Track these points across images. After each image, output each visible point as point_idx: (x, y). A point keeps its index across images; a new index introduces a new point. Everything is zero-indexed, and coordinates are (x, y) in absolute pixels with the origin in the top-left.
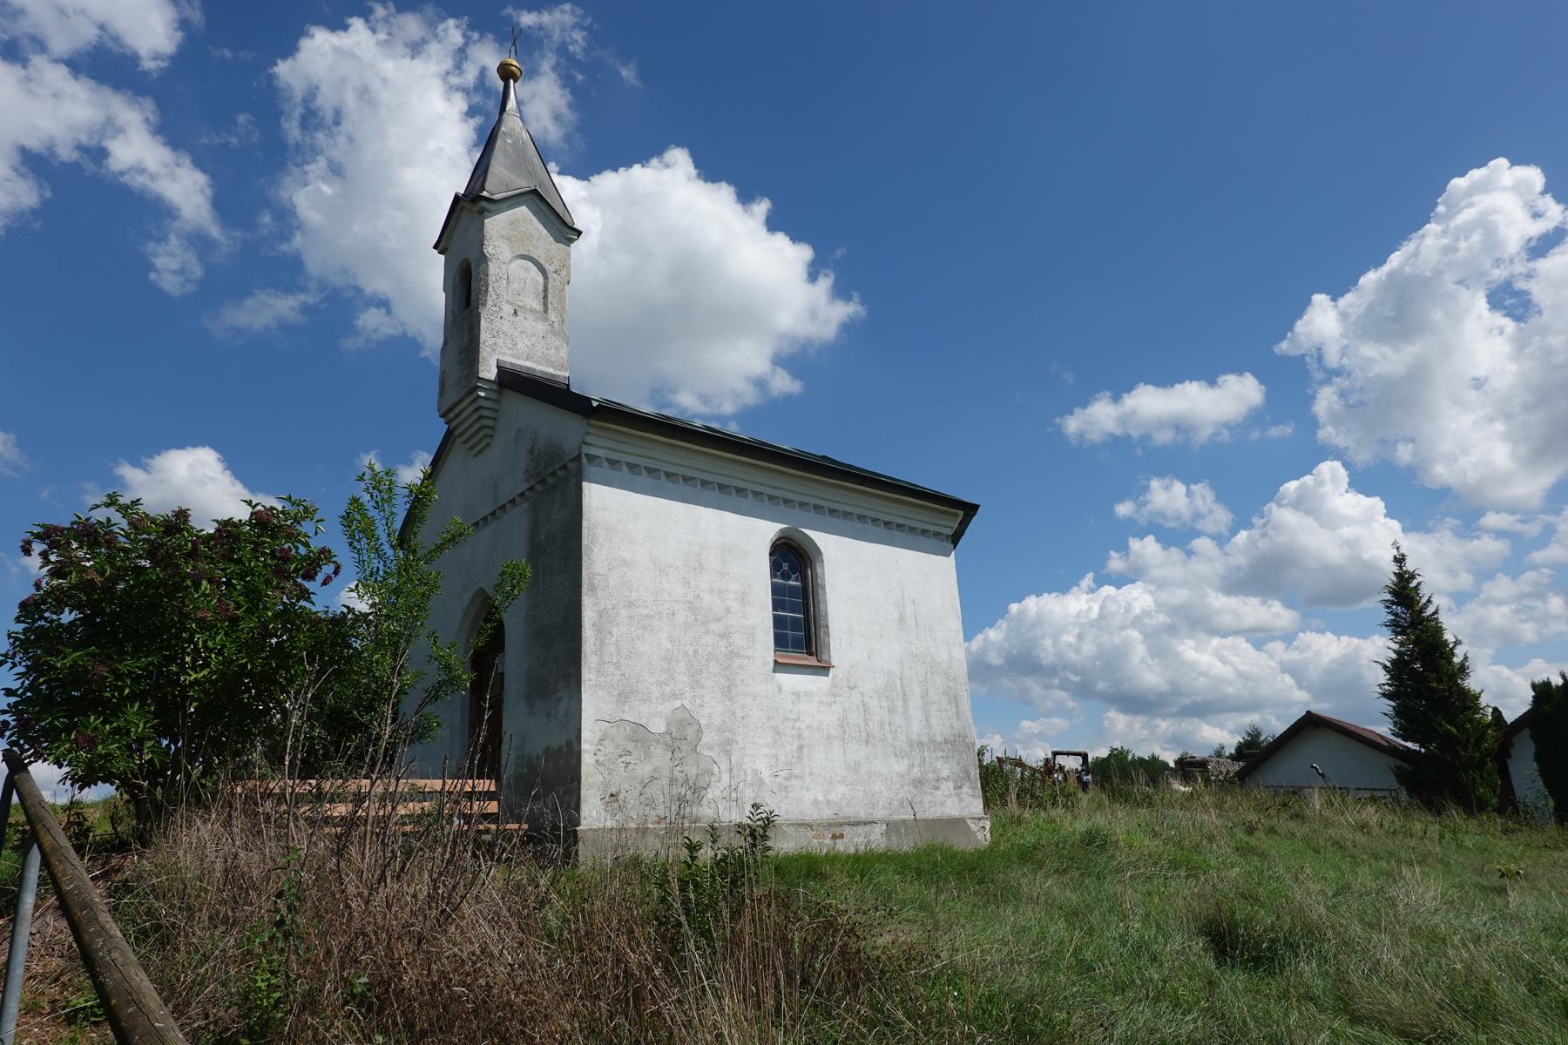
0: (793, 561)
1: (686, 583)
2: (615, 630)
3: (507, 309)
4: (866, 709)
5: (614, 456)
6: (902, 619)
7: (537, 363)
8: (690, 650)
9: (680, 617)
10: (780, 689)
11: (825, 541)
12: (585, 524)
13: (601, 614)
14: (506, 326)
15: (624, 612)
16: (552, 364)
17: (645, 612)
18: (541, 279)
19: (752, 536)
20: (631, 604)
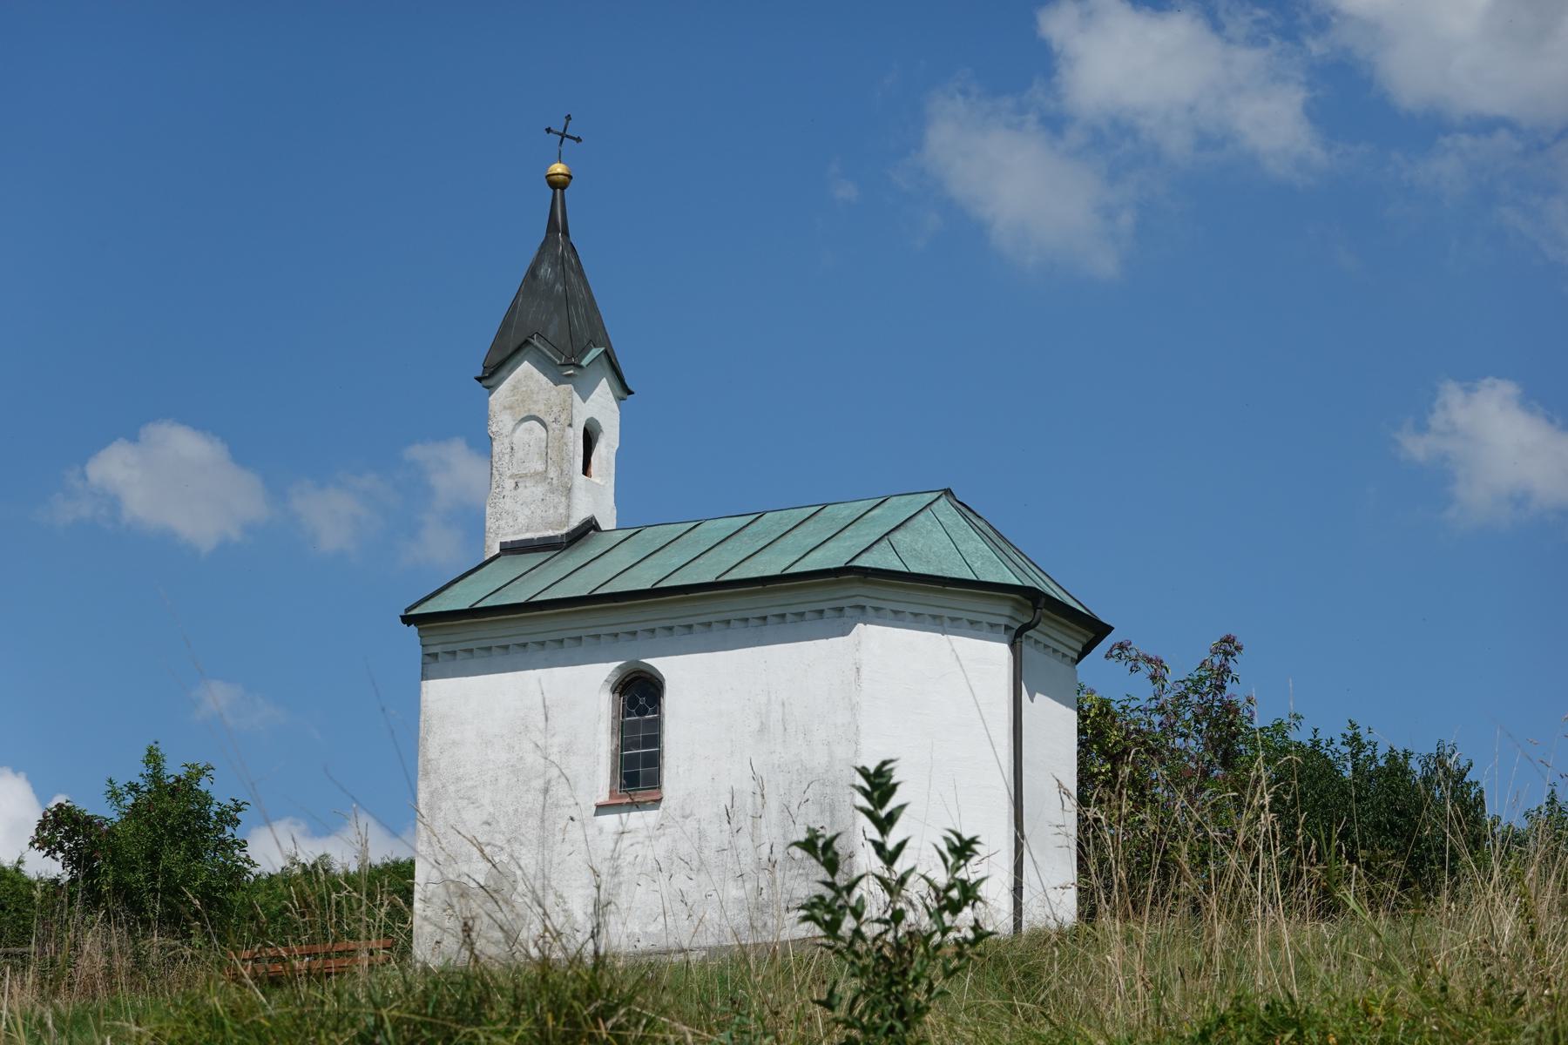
0: (640, 694)
1: (511, 748)
2: (444, 805)
3: (509, 484)
4: (701, 835)
5: (450, 648)
6: (763, 729)
7: (537, 530)
8: (511, 810)
9: (503, 782)
10: (601, 831)
11: (662, 665)
12: (422, 718)
13: (432, 794)
14: (508, 504)
15: (452, 788)
16: (550, 526)
17: (469, 784)
18: (544, 434)
19: (583, 692)
20: (458, 779)
